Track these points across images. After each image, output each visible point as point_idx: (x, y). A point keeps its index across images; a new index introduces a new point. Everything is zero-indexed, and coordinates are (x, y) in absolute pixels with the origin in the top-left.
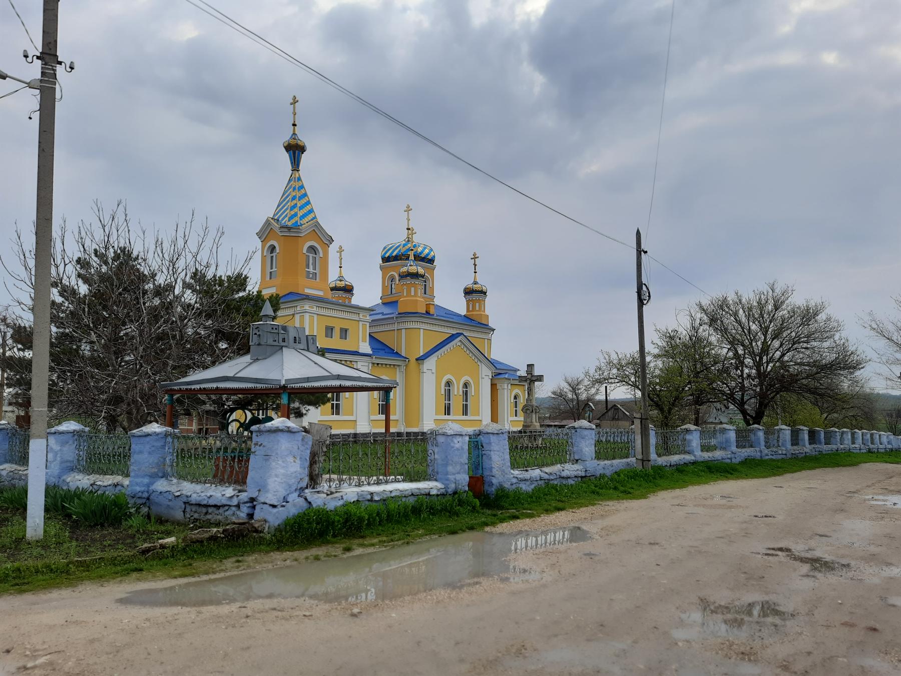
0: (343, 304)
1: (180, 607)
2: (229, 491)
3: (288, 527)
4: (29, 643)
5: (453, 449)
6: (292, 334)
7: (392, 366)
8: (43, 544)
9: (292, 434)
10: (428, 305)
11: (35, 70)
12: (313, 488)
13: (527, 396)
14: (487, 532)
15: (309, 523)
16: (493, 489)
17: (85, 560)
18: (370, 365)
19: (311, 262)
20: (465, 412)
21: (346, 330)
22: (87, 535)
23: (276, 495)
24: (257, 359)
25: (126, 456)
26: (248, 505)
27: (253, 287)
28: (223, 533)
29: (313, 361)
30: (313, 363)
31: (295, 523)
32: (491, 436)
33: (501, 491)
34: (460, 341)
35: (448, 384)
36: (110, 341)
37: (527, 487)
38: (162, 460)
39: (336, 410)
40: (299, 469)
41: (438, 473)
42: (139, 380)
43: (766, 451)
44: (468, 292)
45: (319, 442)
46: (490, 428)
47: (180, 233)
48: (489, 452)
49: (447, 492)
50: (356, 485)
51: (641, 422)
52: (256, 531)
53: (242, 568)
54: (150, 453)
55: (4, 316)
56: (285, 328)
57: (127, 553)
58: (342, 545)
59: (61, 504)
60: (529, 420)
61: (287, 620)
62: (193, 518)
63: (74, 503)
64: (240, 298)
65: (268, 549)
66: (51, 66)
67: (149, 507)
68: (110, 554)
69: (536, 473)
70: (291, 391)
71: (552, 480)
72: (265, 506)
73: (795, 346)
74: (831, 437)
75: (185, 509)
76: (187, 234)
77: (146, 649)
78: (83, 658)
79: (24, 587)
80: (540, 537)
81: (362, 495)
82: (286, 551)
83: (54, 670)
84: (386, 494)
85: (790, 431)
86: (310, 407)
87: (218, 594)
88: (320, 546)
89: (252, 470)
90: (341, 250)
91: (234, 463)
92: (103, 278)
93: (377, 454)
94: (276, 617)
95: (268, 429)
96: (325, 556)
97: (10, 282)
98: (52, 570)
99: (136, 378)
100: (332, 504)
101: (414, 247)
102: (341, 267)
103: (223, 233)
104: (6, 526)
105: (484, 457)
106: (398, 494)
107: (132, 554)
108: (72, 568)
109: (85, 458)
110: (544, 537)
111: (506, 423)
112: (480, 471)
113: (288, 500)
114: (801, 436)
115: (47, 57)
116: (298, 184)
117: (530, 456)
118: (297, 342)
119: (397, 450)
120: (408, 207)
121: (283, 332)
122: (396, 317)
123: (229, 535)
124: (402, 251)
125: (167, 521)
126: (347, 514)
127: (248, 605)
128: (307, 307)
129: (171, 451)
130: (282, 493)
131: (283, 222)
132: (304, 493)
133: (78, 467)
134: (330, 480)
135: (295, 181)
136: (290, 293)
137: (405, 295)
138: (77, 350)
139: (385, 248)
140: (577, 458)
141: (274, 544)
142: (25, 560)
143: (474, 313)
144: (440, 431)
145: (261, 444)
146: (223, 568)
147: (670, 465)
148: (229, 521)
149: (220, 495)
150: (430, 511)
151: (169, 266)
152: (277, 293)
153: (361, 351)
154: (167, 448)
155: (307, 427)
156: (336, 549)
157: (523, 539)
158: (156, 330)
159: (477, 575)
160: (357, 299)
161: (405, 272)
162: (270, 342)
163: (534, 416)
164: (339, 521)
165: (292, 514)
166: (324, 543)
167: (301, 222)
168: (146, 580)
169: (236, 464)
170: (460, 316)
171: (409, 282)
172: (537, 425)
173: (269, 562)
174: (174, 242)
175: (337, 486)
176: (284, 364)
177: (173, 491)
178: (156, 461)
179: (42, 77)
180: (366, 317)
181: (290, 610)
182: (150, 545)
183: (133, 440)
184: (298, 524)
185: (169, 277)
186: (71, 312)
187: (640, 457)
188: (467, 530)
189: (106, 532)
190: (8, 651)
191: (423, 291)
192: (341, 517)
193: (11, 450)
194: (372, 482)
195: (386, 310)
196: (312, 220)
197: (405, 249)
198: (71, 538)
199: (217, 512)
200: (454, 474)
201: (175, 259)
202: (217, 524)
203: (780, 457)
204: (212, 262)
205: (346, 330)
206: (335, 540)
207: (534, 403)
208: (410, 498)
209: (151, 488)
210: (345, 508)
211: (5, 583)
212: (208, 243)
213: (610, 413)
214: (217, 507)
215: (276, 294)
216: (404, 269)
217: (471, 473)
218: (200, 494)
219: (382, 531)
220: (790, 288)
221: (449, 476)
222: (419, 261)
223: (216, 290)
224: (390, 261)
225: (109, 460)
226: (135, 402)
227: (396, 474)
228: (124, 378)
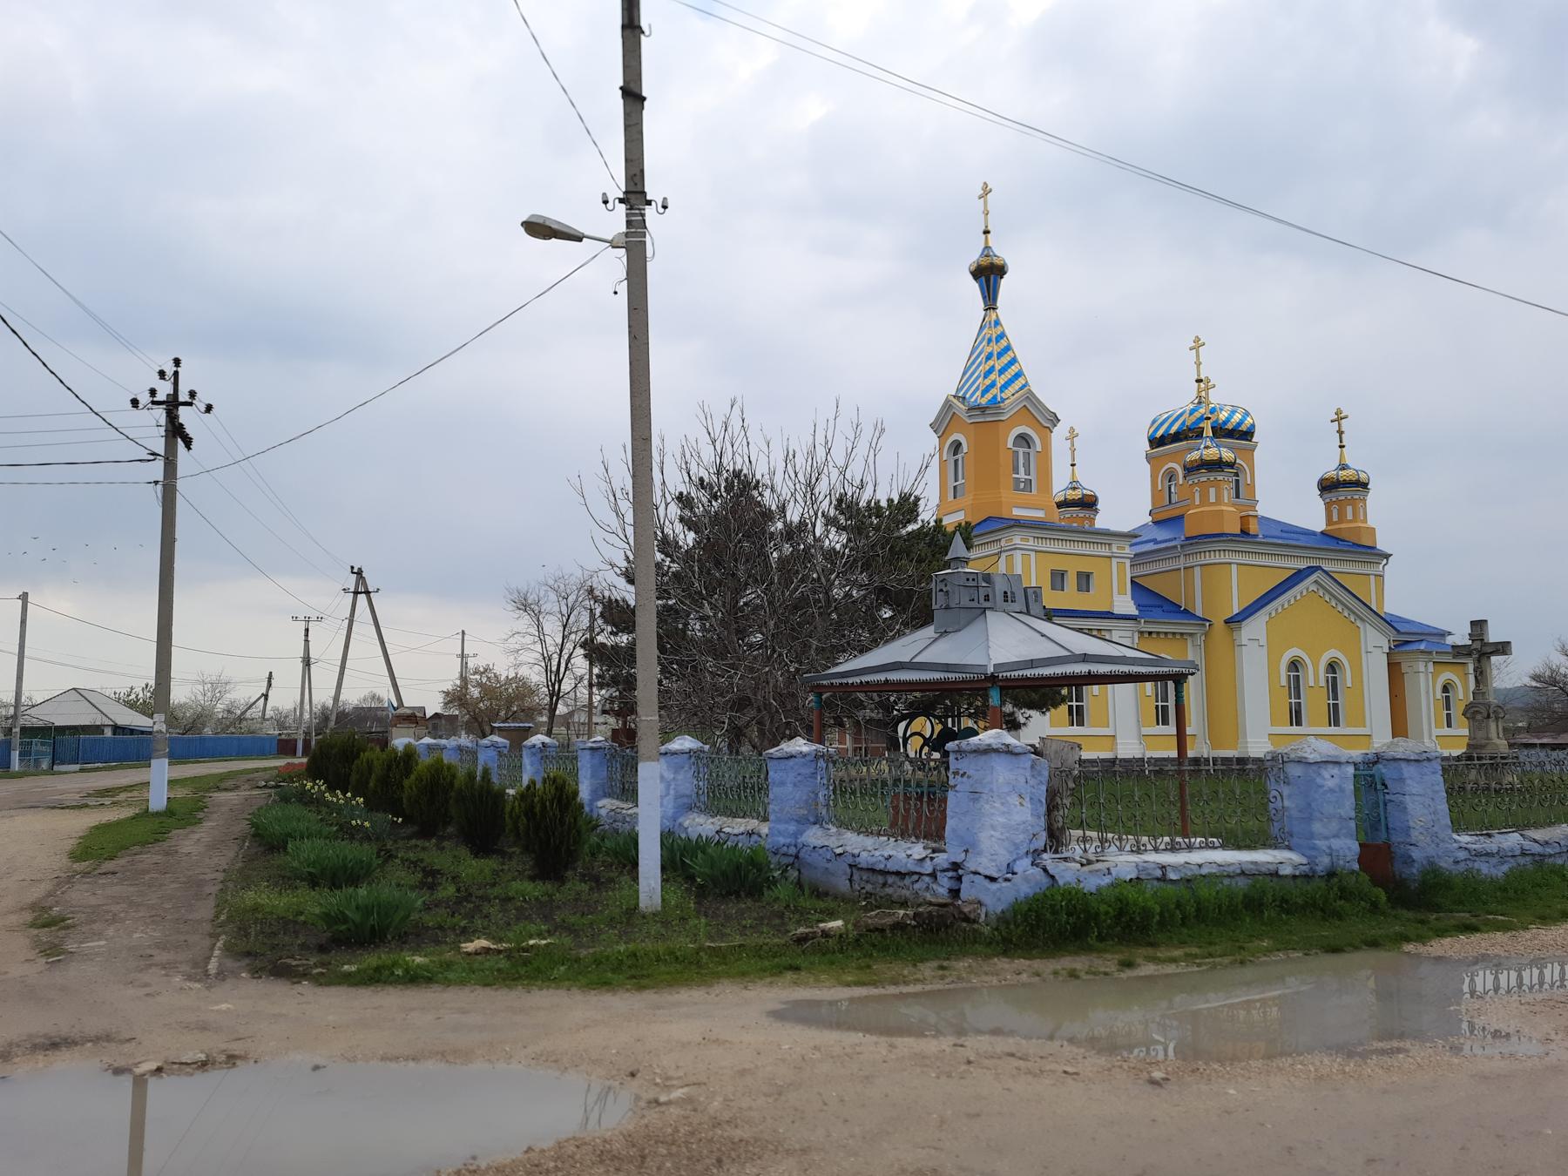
0: (1080, 529)
1: (861, 1035)
2: (918, 850)
3: (1019, 917)
4: (658, 1065)
5: (1321, 790)
6: (1000, 586)
8: (662, 917)
9: (1013, 757)
10: (1244, 520)
11: (616, 222)
12: (1056, 852)
13: (1472, 685)
14: (1409, 952)
15: (1054, 913)
16: (1415, 871)
17: (720, 947)
18: (1136, 635)
19: (1021, 461)
20: (1334, 719)
22: (718, 909)
23: (995, 860)
24: (945, 632)
25: (762, 789)
26: (950, 874)
27: (927, 514)
28: (914, 918)
29: (1038, 632)
30: (1038, 635)
31: (1030, 910)
32: (1403, 765)
33: (1432, 875)
35: (1294, 665)
36: (729, 614)
37: (1492, 869)
38: (813, 796)
39: (1077, 716)
40: (1030, 818)
41: (1291, 836)
42: (772, 673)
44: (1328, 486)
45: (1061, 772)
46: (1401, 750)
47: (820, 439)
48: (1401, 798)
49: (1314, 872)
50: (1132, 851)
52: (967, 919)
53: (950, 979)
54: (795, 785)
55: (591, 587)
56: (988, 578)
57: (776, 940)
58: (1117, 957)
59: (681, 859)
60: (1480, 734)
61: (1035, 1076)
62: (864, 891)
63: (696, 858)
64: (909, 534)
65: (989, 951)
66: (639, 209)
67: (799, 870)
68: (754, 940)
69: (1512, 840)
70: (1004, 684)
71: (1551, 855)
72: (978, 879)
75: (852, 876)
76: (829, 438)
77: (820, 1094)
78: (732, 1098)
79: (644, 982)
80: (1528, 971)
81: (1145, 869)
82: (1019, 957)
83: (695, 1110)
84: (1191, 870)
86: (1032, 713)
87: (912, 1020)
88: (1076, 953)
89: (952, 818)
90: (1072, 435)
91: (922, 804)
92: (716, 519)
93: (1168, 795)
94: (1016, 1068)
95: (974, 748)
96: (1087, 973)
97: (599, 534)
98: (677, 958)
99: (767, 669)
100: (1092, 883)
101: (1211, 413)
102: (1073, 465)
103: (883, 430)
104: (613, 890)
105: (1389, 807)
106: (1214, 871)
107: (783, 942)
108: (704, 957)
109: (706, 791)
110: (1536, 972)
112: (1383, 835)
113: (1015, 870)
115: (632, 197)
116: (995, 332)
117: (1496, 806)
118: (1009, 599)
119: (1205, 790)
120: (1197, 339)
121: (984, 584)
122: (1182, 546)
123: (924, 923)
124: (1189, 423)
125: (827, 894)
126: (1120, 900)
127: (966, 1044)
128: (1016, 539)
129: (825, 782)
130: (1004, 857)
131: (972, 400)
132: (1041, 859)
133: (698, 805)
134: (1085, 840)
135: (990, 327)
137: (1197, 502)
138: (684, 631)
141: (998, 943)
142: (643, 941)
143: (1343, 526)
144: (1292, 756)
145: (966, 773)
146: (919, 976)
148: (921, 900)
149: (904, 855)
150: (1281, 906)
151: (807, 492)
152: (969, 520)
153: (1117, 611)
154: (819, 778)
155: (1037, 745)
156: (1107, 962)
157: (1488, 972)
158: (790, 595)
159: (1387, 1035)
160: (1105, 519)
161: (1196, 460)
162: (965, 602)
163: (1493, 726)
164: (1107, 913)
165: (1023, 895)
166: (1083, 949)
167: (1003, 395)
168: (806, 984)
169: (925, 805)
170: (1314, 533)
171: (1205, 479)
172: (1501, 745)
173: (992, 974)
174: (812, 454)
175: (1099, 850)
176: (990, 638)
177: (832, 846)
178: (804, 798)
179: (627, 228)
181: (1039, 1060)
182: (807, 930)
183: (771, 764)
184: (1036, 912)
185: (806, 510)
186: (675, 575)
188: (1364, 947)
189: (743, 906)
190: (633, 1075)
191: (1233, 492)
192: (1110, 906)
193: (611, 779)
194: (1162, 847)
195: (1162, 534)
196: (1021, 389)
197: (1193, 419)
198: (698, 912)
199: (901, 884)
200: (1327, 838)
201: (814, 480)
202: (904, 904)
204: (869, 479)
206: (1101, 945)
207: (1492, 699)
208: (1238, 878)
209: (799, 841)
210: (1117, 890)
211: (619, 974)
212: (862, 449)
214: (900, 875)
215: (966, 523)
216: (1195, 455)
217: (1363, 837)
218: (873, 852)
219: (1190, 936)
221: (1317, 842)
222: (1224, 437)
223: (872, 523)
224: (1165, 444)
225: (739, 796)
226: (767, 706)
227: (1207, 835)
228: (751, 670)
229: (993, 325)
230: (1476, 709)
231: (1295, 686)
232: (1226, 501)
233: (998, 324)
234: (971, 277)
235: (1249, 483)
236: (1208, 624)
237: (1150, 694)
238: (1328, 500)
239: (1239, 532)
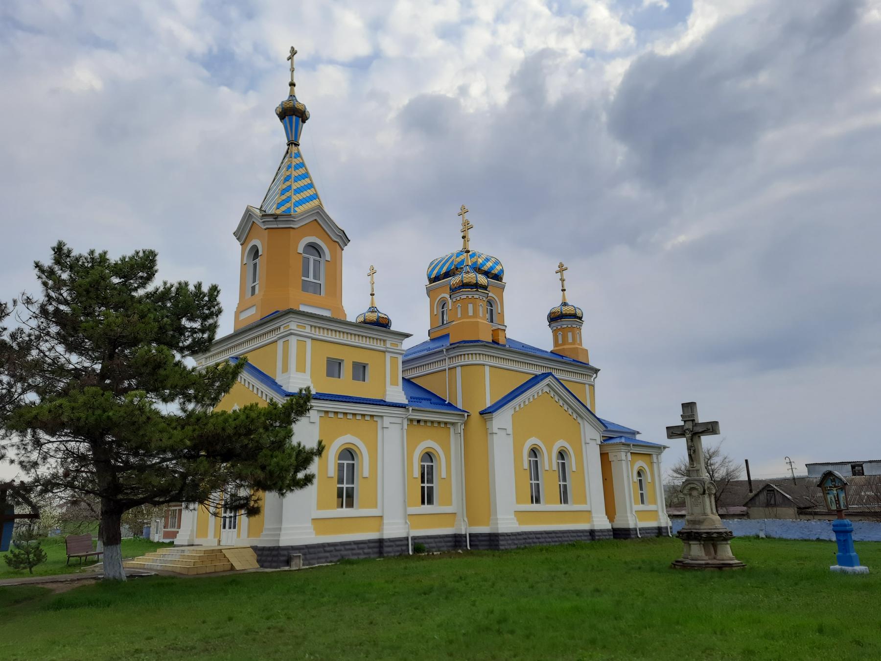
10: (495, 332)
18: (406, 423)
20: (564, 499)
21: (364, 367)
44: (554, 318)
111: (629, 515)
116: (297, 161)
122: (447, 350)
124: (455, 263)
137: (459, 316)
139: (431, 264)
143: (565, 347)
153: (389, 399)
171: (465, 297)
213: (763, 497)
230: (692, 486)
231: (535, 467)
232: (481, 315)
235: (499, 312)
236: (466, 414)
237: (417, 477)
238: (555, 328)
239: (491, 341)
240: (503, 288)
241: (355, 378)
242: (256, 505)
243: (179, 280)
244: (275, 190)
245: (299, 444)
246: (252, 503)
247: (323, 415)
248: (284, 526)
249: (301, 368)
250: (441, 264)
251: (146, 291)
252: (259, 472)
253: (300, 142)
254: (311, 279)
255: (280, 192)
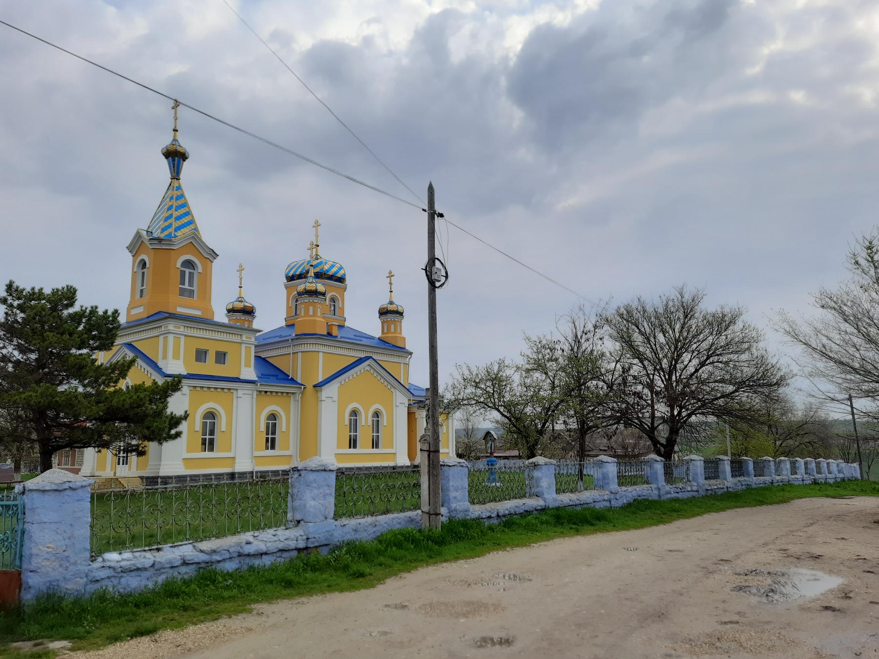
7: (285, 395)
18: (255, 393)
20: (375, 444)
21: (225, 354)
34: (369, 365)
35: (354, 413)
43: (668, 488)
44: (383, 312)
51: (429, 455)
71: (219, 562)
73: (711, 359)
74: (764, 466)
85: (702, 463)
114: (721, 467)
135: (173, 190)
136: (159, 313)
137: (303, 315)
139: (289, 266)
140: (298, 517)
147: (498, 516)
153: (242, 377)
170: (372, 338)
180: (179, 328)
187: (426, 508)
203: (689, 495)
205: (225, 354)
220: (700, 292)
229: (175, 189)
231: (354, 425)
232: (319, 315)
233: (179, 189)
234: (164, 157)
236: (303, 387)
240: (345, 289)
241: (217, 362)
242: (143, 450)
243: (91, 305)
244: (160, 216)
245: (172, 413)
246: (140, 449)
247: (192, 389)
248: (162, 463)
249: (176, 356)
250: (297, 267)
251: (68, 311)
252: (146, 431)
253: (181, 177)
254: (186, 286)
255: (164, 219)
